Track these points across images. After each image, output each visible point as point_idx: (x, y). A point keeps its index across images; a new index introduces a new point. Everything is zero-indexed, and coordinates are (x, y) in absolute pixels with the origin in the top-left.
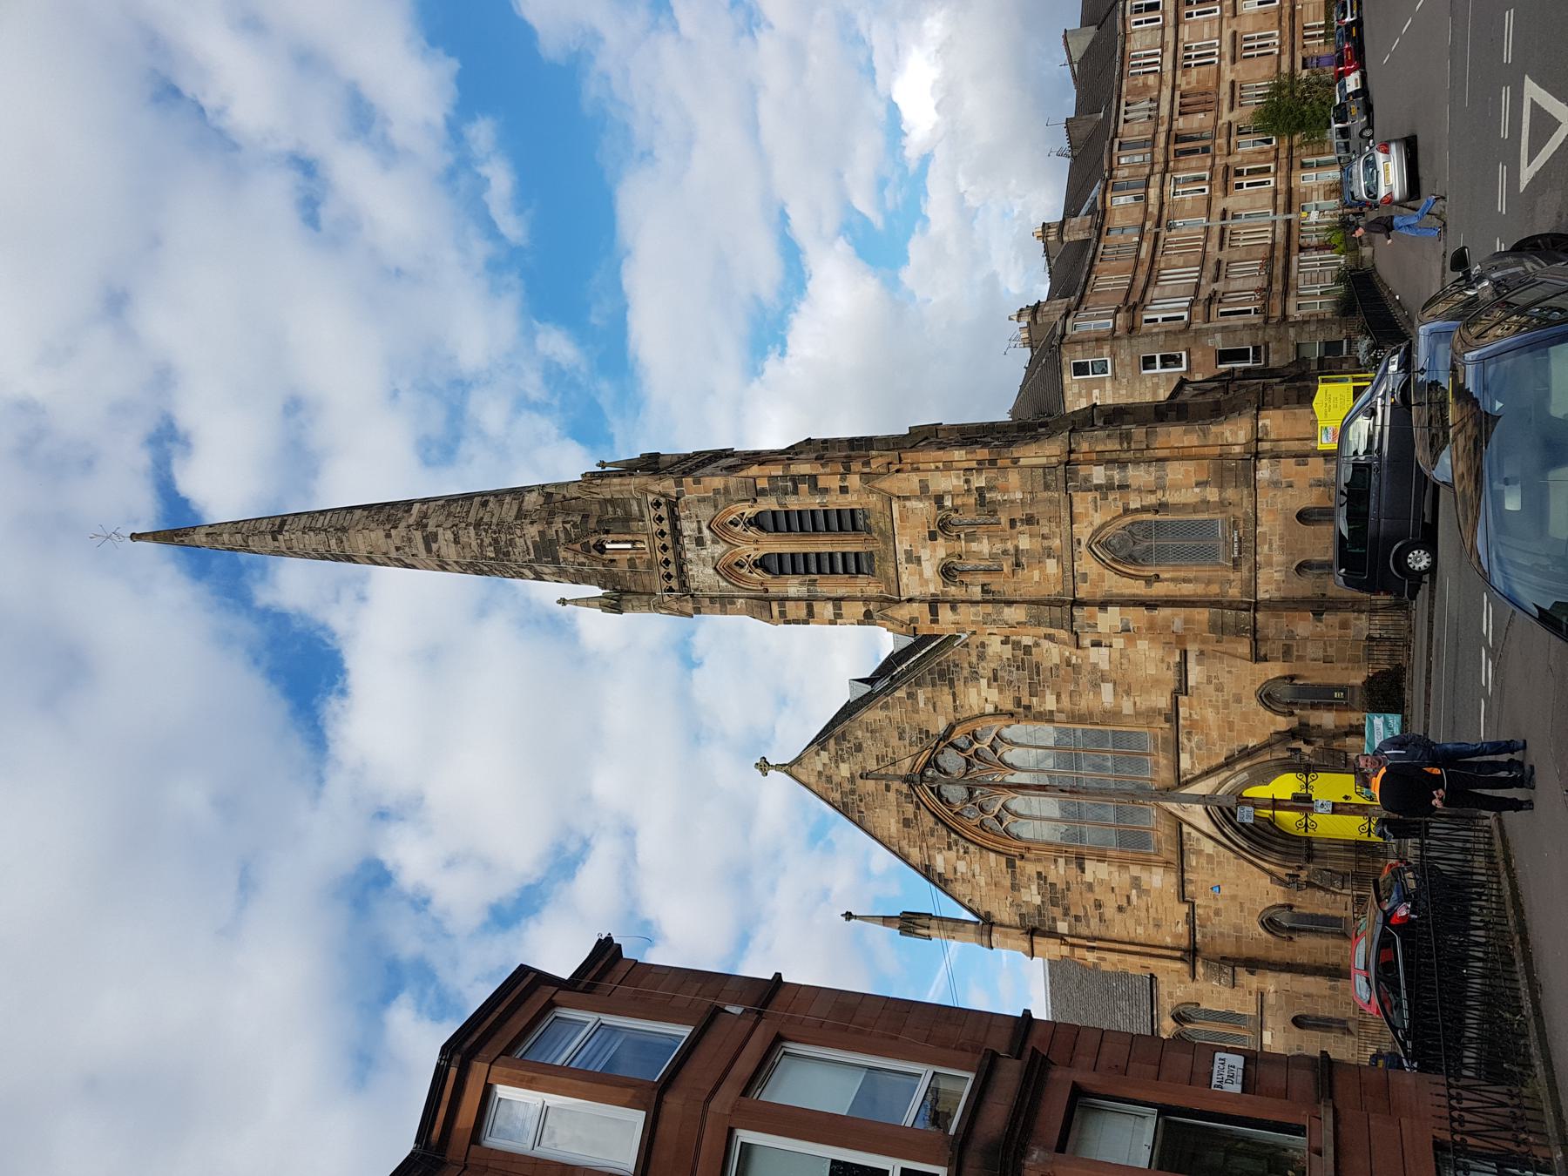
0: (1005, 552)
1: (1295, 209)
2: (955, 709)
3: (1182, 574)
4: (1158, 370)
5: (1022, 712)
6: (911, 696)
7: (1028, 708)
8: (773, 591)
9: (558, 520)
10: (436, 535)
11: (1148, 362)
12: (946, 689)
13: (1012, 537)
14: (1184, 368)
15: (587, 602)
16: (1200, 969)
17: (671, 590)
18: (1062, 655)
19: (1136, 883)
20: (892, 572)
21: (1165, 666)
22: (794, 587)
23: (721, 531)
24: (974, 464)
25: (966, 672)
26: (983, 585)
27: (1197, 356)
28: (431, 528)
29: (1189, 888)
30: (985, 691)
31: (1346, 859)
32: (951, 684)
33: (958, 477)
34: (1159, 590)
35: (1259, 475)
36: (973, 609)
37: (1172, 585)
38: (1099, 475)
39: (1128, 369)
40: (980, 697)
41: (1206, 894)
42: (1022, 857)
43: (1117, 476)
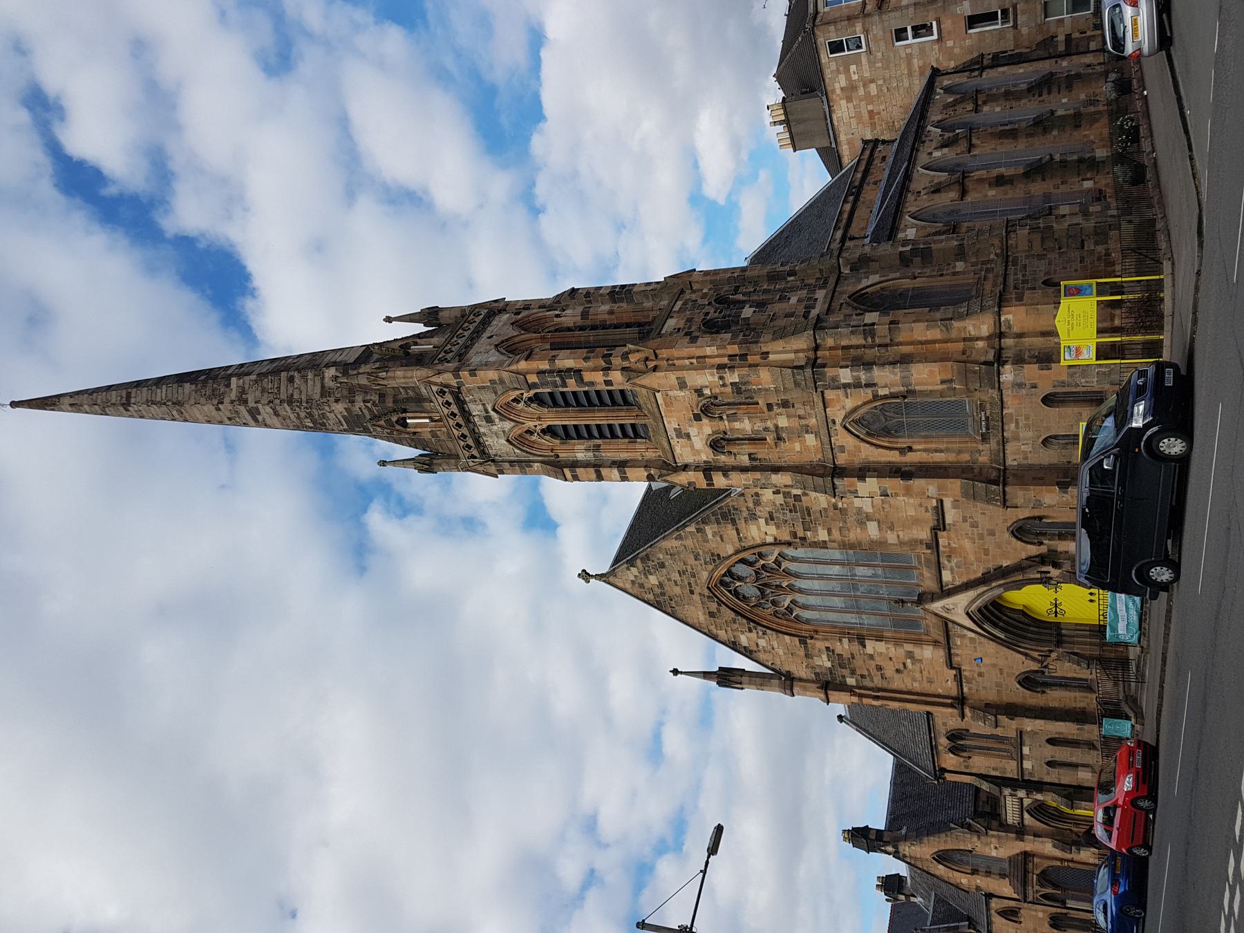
0: (766, 429)
1: (764, 434)
2: (740, 539)
3: (934, 446)
4: (911, 41)
5: (797, 541)
6: (699, 530)
7: (804, 539)
8: (563, 455)
9: (359, 398)
10: (257, 409)
11: (900, 34)
12: (730, 526)
13: (770, 418)
14: (935, 37)
15: (404, 462)
16: (967, 711)
17: (473, 457)
18: (829, 502)
19: (910, 655)
20: (666, 444)
21: (923, 509)
22: (580, 451)
23: (505, 411)
24: (725, 360)
25: (745, 514)
26: (750, 455)
27: (947, 25)
28: (251, 404)
29: (956, 659)
30: (764, 528)
31: (1091, 644)
32: (734, 522)
33: (712, 375)
34: (911, 457)
35: (1003, 378)
36: (743, 476)
37: (924, 455)
38: (846, 375)
39: (882, 43)
40: (760, 531)
41: (970, 663)
42: (812, 638)
43: (863, 376)
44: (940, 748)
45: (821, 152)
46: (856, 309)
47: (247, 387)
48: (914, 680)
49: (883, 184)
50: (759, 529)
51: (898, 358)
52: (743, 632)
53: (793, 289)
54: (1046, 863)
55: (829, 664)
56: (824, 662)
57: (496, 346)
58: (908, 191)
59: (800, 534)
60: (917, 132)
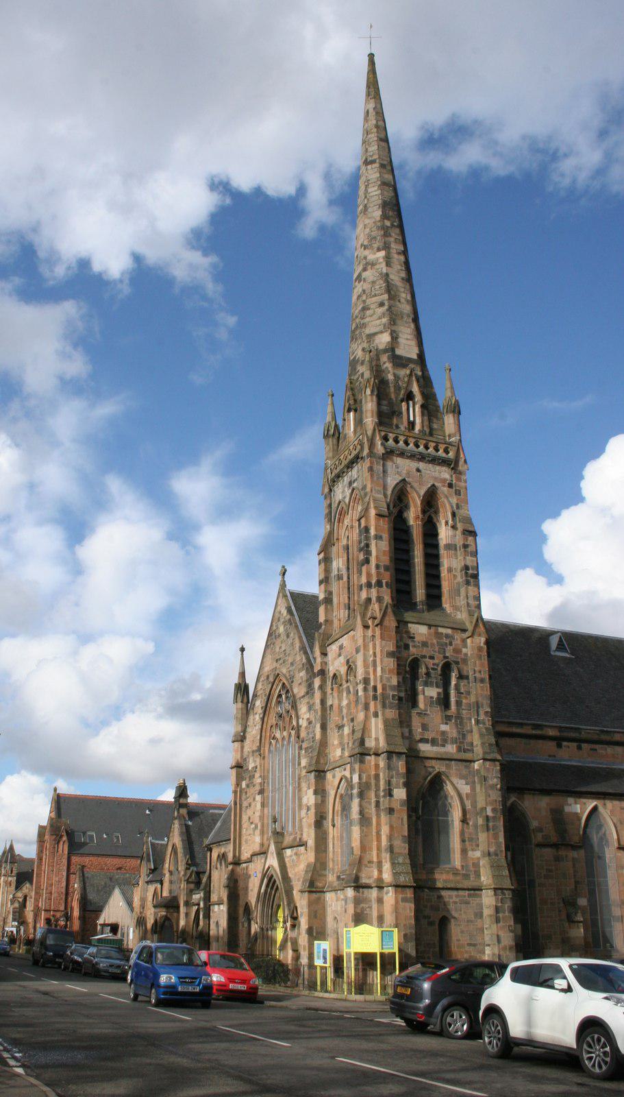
51: (367, 815)
54: (174, 921)
55: (250, 769)
56: (251, 766)
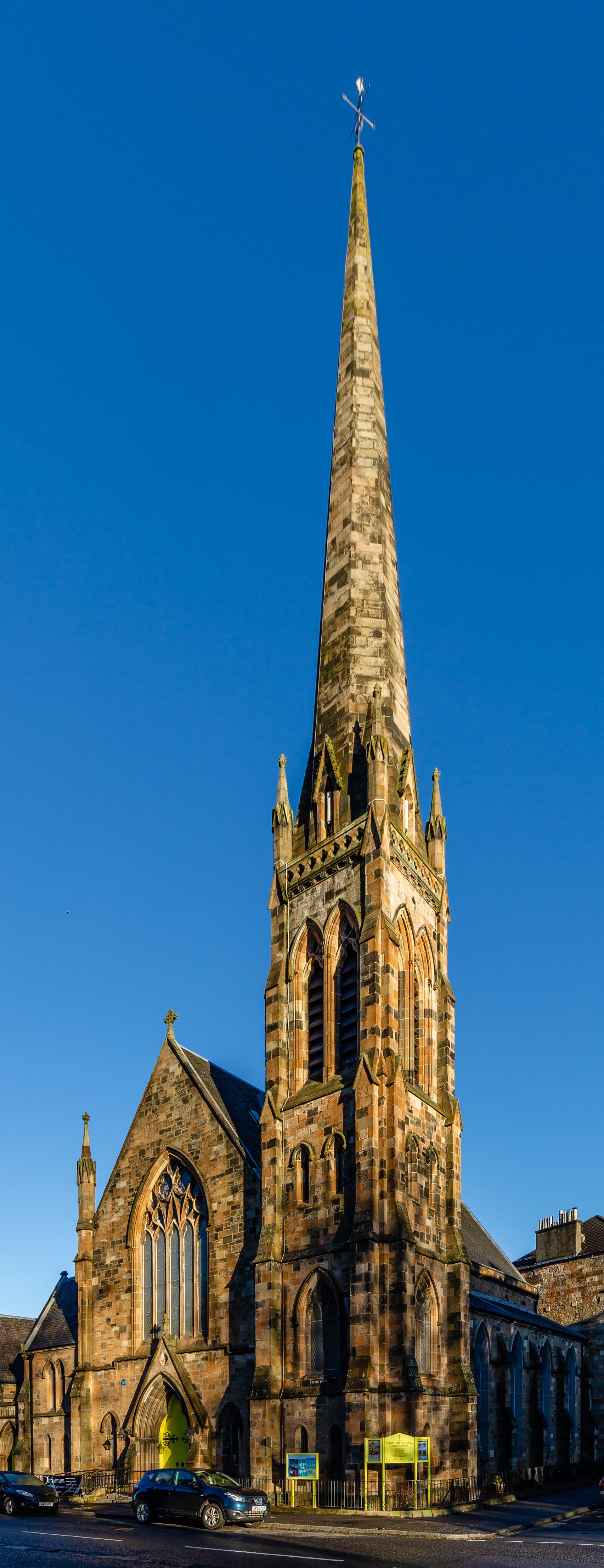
1: (311, 1199)
29: (123, 1364)
32: (229, 1171)
44: (50, 1354)
45: (533, 1254)
46: (418, 1278)
47: (371, 567)
48: (103, 1333)
49: (505, 1303)
50: (224, 1196)
52: (129, 1183)
53: (438, 1222)
55: (108, 1262)
57: (404, 906)
58: (502, 1321)
59: (221, 1234)
60: (544, 1328)
